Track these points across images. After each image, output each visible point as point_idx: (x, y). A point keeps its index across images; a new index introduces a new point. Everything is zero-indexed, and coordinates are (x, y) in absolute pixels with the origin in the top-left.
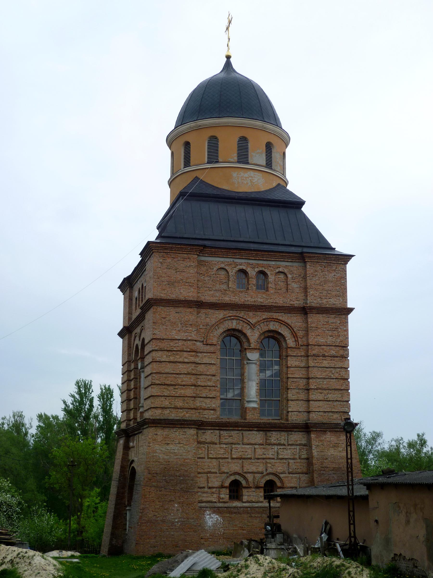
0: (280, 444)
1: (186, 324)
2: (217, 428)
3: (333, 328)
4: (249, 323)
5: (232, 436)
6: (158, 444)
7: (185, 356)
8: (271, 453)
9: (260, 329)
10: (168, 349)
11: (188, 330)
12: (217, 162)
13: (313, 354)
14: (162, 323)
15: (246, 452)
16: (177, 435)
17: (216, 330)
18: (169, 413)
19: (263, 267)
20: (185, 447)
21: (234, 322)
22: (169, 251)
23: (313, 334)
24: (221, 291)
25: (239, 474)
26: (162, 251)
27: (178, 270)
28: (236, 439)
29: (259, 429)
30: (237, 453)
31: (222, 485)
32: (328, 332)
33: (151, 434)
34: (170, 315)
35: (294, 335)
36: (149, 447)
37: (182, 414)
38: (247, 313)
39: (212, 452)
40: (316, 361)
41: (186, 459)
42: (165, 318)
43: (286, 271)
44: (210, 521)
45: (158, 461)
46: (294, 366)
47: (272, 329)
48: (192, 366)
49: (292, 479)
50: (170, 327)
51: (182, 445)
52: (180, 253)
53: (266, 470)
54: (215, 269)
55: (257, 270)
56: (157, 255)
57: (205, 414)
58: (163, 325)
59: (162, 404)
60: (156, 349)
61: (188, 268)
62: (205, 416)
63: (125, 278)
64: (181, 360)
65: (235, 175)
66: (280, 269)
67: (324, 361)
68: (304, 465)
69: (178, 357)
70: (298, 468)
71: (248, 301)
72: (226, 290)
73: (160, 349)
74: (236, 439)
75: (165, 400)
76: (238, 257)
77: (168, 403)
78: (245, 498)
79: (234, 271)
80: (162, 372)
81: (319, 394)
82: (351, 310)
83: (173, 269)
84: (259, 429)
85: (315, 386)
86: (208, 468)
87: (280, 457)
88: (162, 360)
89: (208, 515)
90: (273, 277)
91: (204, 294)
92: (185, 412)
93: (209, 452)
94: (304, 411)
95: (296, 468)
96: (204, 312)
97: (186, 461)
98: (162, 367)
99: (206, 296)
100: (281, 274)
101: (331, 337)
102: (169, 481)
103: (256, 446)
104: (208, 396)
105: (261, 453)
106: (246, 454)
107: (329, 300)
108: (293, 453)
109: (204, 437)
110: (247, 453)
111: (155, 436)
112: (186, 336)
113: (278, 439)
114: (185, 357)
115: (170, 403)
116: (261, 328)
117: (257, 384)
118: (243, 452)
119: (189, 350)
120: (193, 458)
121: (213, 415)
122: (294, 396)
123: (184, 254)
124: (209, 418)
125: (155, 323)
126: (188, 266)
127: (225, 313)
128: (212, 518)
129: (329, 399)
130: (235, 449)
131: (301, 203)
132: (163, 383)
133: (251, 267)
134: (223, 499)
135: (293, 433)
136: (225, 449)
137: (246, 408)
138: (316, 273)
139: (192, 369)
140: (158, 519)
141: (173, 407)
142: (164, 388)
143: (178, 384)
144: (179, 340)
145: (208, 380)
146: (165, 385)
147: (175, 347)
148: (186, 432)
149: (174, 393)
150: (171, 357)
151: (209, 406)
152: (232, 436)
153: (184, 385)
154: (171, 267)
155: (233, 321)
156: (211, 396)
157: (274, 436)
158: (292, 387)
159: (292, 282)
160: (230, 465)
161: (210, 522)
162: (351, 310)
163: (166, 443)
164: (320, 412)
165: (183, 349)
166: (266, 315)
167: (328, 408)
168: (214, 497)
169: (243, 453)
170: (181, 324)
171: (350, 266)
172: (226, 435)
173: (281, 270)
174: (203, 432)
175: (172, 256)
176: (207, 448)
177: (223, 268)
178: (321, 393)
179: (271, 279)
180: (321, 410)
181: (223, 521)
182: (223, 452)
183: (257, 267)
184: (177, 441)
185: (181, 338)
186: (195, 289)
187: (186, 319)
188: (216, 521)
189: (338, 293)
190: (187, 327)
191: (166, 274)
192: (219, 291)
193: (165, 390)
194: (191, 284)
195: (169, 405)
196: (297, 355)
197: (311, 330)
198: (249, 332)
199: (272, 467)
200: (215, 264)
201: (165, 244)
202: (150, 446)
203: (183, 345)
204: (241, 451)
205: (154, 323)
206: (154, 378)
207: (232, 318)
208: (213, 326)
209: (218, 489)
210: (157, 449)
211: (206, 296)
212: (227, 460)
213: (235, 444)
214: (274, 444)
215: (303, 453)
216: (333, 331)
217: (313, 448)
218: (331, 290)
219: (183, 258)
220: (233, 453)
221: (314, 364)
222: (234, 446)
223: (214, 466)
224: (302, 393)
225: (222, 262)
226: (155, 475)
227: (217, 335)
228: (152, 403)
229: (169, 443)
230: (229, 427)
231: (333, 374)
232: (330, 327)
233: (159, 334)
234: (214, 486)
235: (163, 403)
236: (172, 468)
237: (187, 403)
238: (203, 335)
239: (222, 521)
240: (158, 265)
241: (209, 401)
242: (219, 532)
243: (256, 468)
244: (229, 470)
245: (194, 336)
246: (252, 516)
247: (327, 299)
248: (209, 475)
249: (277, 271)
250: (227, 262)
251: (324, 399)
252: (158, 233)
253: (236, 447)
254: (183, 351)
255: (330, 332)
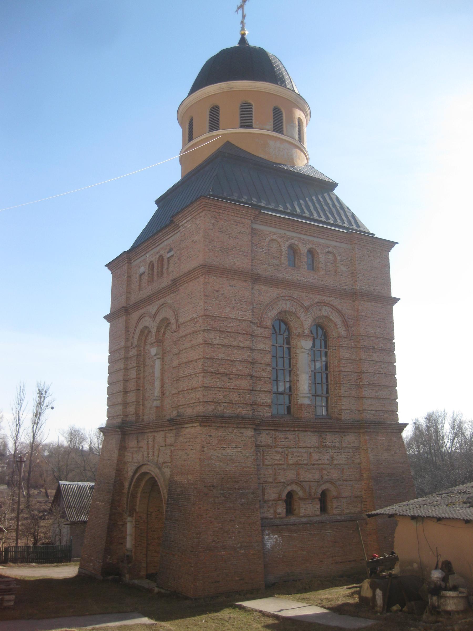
0: (334, 447)
1: (240, 301)
2: (272, 428)
3: (380, 319)
4: (302, 306)
5: (288, 438)
6: (213, 449)
7: (240, 339)
8: (326, 458)
9: (313, 314)
10: (221, 330)
11: (242, 307)
12: (251, 127)
13: (365, 346)
14: (215, 297)
15: (302, 456)
16: (234, 436)
17: (270, 311)
18: (223, 409)
19: (313, 244)
20: (243, 452)
21: (288, 303)
22: (222, 211)
23: (364, 324)
24: (274, 266)
25: (296, 483)
26: (214, 210)
27: (231, 235)
28: (292, 442)
29: (315, 430)
30: (293, 458)
31: (279, 497)
32: (376, 322)
33: (205, 436)
34: (223, 288)
35: (345, 323)
36: (203, 453)
37: (238, 411)
38: (300, 294)
39: (268, 457)
40: (367, 354)
41: (245, 467)
42: (217, 291)
43: (335, 252)
44: (269, 542)
45: (214, 471)
46: (346, 358)
47: (324, 314)
48: (248, 352)
49: (346, 487)
50: (224, 303)
51: (239, 450)
52: (233, 216)
53: (322, 478)
54: (267, 240)
55: (308, 246)
56: (209, 215)
57: (260, 412)
58: (216, 299)
59: (215, 398)
60: (208, 328)
61: (241, 234)
62: (260, 413)
63: (124, 252)
64: (235, 343)
65: (271, 143)
66: (330, 249)
67: (374, 354)
68: (357, 471)
69: (232, 340)
70: (352, 475)
71: (300, 280)
72: (277, 265)
73: (213, 328)
74: (292, 442)
75: (218, 392)
76: (290, 229)
77: (221, 397)
78: (302, 512)
79: (286, 245)
80: (215, 357)
81: (371, 391)
82: (396, 300)
83: (226, 233)
84: (315, 430)
85: (367, 381)
86: (264, 477)
87: (335, 462)
88: (214, 343)
89: (266, 536)
90: (323, 257)
91: (257, 268)
92: (241, 409)
93: (265, 457)
94: (356, 409)
95: (350, 475)
96: (257, 288)
97: (245, 469)
98: (215, 351)
99: (258, 270)
100: (329, 254)
101: (379, 329)
102: (227, 496)
103: (312, 450)
104: (262, 390)
105: (317, 458)
106: (303, 459)
107: (376, 288)
108: (347, 457)
109: (259, 439)
110: (304, 458)
111: (209, 438)
112: (241, 315)
113: (332, 441)
114: (240, 341)
115: (224, 397)
116: (314, 312)
117: (310, 377)
118: (299, 456)
119: (244, 332)
120: (252, 466)
121: (268, 412)
122: (346, 393)
123: (238, 217)
124: (264, 416)
125: (207, 296)
126: (242, 232)
127: (278, 291)
128: (271, 538)
129: (379, 397)
130: (291, 454)
131: (333, 185)
132: (217, 371)
133: (303, 243)
134: (280, 514)
135: (346, 434)
136: (281, 454)
137: (301, 405)
138: (364, 257)
139: (248, 356)
140: (218, 545)
141: (227, 402)
142: (218, 378)
143: (232, 373)
144: (233, 319)
145: (263, 370)
146: (218, 373)
147: (229, 327)
148: (242, 433)
149: (228, 384)
150: (225, 340)
151: (264, 401)
152: (288, 438)
153: (239, 375)
154: (224, 230)
155: (287, 302)
156: (266, 390)
157: (330, 439)
158: (344, 382)
159: (341, 264)
160: (286, 473)
161: (269, 544)
162: (396, 300)
163: (221, 447)
164: (372, 410)
165: (238, 331)
166: (318, 298)
167: (379, 407)
168: (270, 513)
169: (299, 458)
170: (235, 300)
171: (393, 254)
172: (282, 436)
173: (330, 249)
174: (258, 434)
175: (225, 218)
176: (262, 453)
177: (275, 240)
178: (372, 390)
179: (322, 259)
180: (373, 409)
181: (283, 541)
182: (279, 458)
183: (308, 244)
184: (234, 445)
185: (235, 317)
186: (249, 260)
187: (240, 295)
188: (275, 542)
189: (383, 281)
190: (242, 304)
191: (218, 238)
192: (272, 266)
193: (218, 380)
194: (244, 254)
195: (223, 398)
196: (348, 346)
197: (361, 319)
198: (302, 316)
199: (328, 474)
200: (267, 234)
201: (219, 202)
202: (204, 451)
203: (237, 326)
204: (297, 456)
205: (206, 296)
206: (206, 364)
207: (287, 298)
208: (267, 306)
209: (274, 502)
210: (212, 455)
211: (258, 270)
212: (283, 466)
213: (290, 447)
214: (329, 447)
215: (356, 458)
216: (381, 321)
217: (369, 452)
218: (376, 278)
219: (236, 222)
220: (289, 458)
221: (365, 357)
222: (289, 450)
223: (270, 475)
224: (354, 389)
225: (275, 234)
226: (212, 488)
227: (271, 317)
228: (204, 396)
229: (225, 447)
230: (285, 427)
231: (382, 369)
232: (378, 317)
233: (211, 310)
234: (270, 499)
235: (217, 397)
236: (230, 478)
237: (243, 397)
238: (257, 316)
239: (281, 541)
240: (210, 226)
241: (264, 396)
242: (279, 555)
243: (313, 476)
244: (286, 479)
245: (248, 315)
246: (311, 534)
247: (373, 286)
248: (264, 485)
249: (327, 250)
250: (278, 234)
251: (376, 396)
252: (157, 208)
253: (293, 451)
254: (237, 333)
255: (378, 322)
